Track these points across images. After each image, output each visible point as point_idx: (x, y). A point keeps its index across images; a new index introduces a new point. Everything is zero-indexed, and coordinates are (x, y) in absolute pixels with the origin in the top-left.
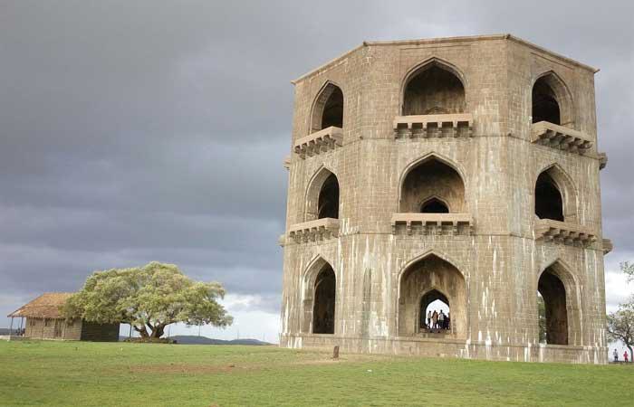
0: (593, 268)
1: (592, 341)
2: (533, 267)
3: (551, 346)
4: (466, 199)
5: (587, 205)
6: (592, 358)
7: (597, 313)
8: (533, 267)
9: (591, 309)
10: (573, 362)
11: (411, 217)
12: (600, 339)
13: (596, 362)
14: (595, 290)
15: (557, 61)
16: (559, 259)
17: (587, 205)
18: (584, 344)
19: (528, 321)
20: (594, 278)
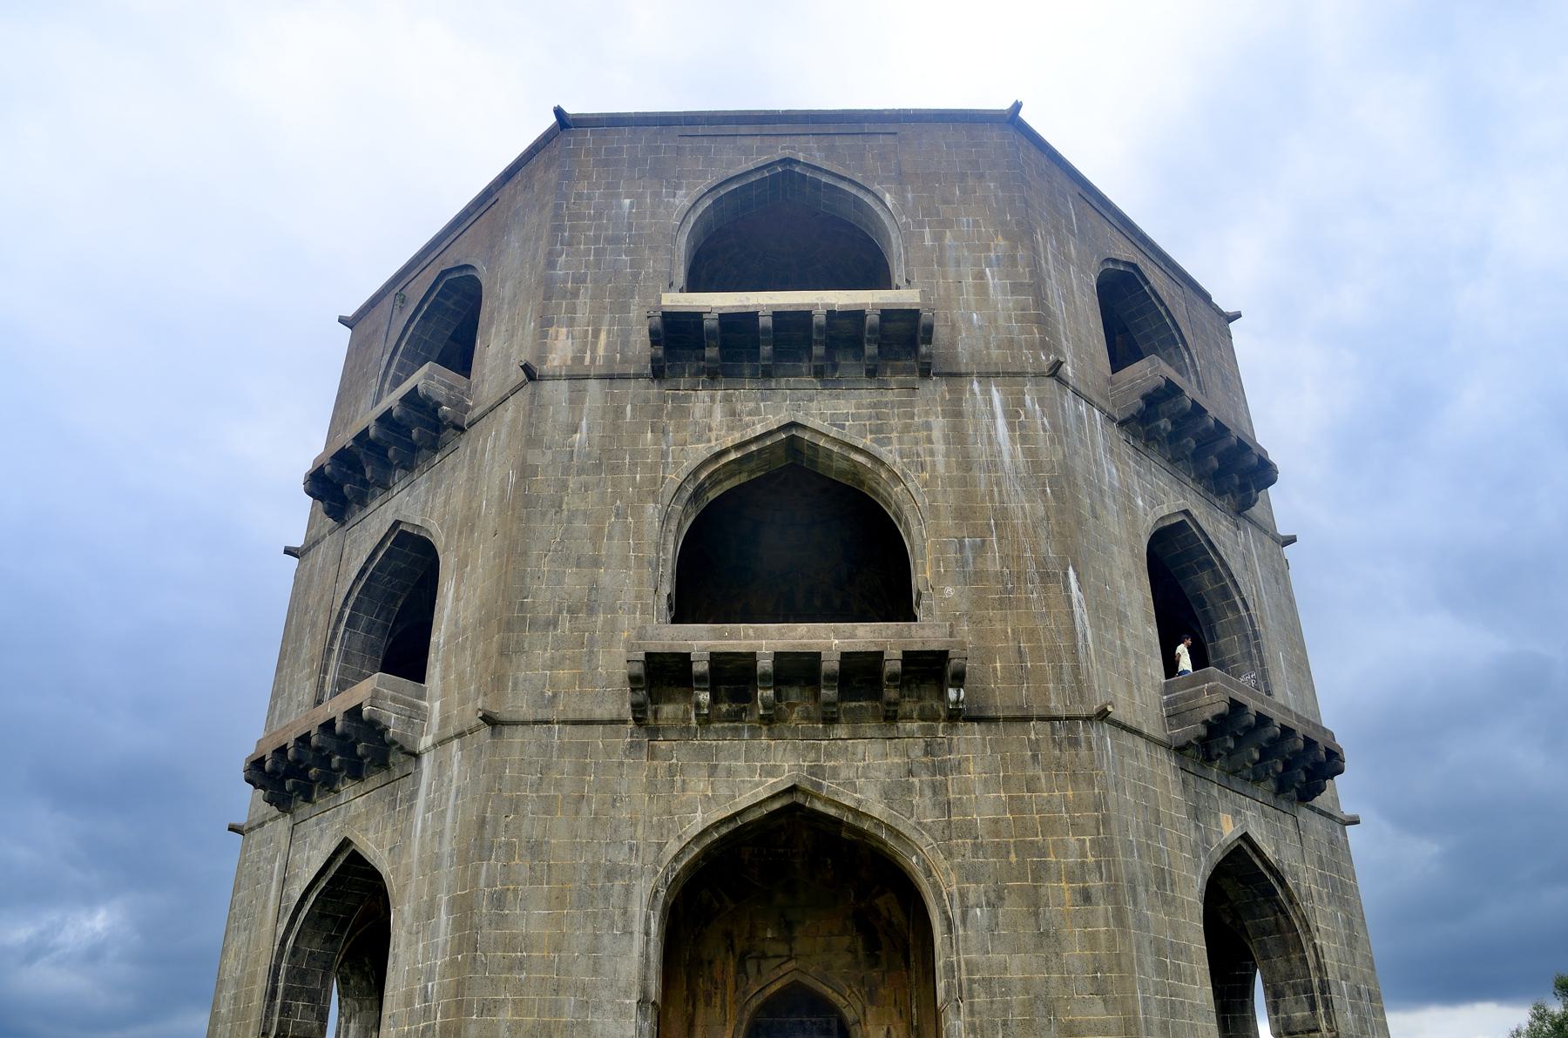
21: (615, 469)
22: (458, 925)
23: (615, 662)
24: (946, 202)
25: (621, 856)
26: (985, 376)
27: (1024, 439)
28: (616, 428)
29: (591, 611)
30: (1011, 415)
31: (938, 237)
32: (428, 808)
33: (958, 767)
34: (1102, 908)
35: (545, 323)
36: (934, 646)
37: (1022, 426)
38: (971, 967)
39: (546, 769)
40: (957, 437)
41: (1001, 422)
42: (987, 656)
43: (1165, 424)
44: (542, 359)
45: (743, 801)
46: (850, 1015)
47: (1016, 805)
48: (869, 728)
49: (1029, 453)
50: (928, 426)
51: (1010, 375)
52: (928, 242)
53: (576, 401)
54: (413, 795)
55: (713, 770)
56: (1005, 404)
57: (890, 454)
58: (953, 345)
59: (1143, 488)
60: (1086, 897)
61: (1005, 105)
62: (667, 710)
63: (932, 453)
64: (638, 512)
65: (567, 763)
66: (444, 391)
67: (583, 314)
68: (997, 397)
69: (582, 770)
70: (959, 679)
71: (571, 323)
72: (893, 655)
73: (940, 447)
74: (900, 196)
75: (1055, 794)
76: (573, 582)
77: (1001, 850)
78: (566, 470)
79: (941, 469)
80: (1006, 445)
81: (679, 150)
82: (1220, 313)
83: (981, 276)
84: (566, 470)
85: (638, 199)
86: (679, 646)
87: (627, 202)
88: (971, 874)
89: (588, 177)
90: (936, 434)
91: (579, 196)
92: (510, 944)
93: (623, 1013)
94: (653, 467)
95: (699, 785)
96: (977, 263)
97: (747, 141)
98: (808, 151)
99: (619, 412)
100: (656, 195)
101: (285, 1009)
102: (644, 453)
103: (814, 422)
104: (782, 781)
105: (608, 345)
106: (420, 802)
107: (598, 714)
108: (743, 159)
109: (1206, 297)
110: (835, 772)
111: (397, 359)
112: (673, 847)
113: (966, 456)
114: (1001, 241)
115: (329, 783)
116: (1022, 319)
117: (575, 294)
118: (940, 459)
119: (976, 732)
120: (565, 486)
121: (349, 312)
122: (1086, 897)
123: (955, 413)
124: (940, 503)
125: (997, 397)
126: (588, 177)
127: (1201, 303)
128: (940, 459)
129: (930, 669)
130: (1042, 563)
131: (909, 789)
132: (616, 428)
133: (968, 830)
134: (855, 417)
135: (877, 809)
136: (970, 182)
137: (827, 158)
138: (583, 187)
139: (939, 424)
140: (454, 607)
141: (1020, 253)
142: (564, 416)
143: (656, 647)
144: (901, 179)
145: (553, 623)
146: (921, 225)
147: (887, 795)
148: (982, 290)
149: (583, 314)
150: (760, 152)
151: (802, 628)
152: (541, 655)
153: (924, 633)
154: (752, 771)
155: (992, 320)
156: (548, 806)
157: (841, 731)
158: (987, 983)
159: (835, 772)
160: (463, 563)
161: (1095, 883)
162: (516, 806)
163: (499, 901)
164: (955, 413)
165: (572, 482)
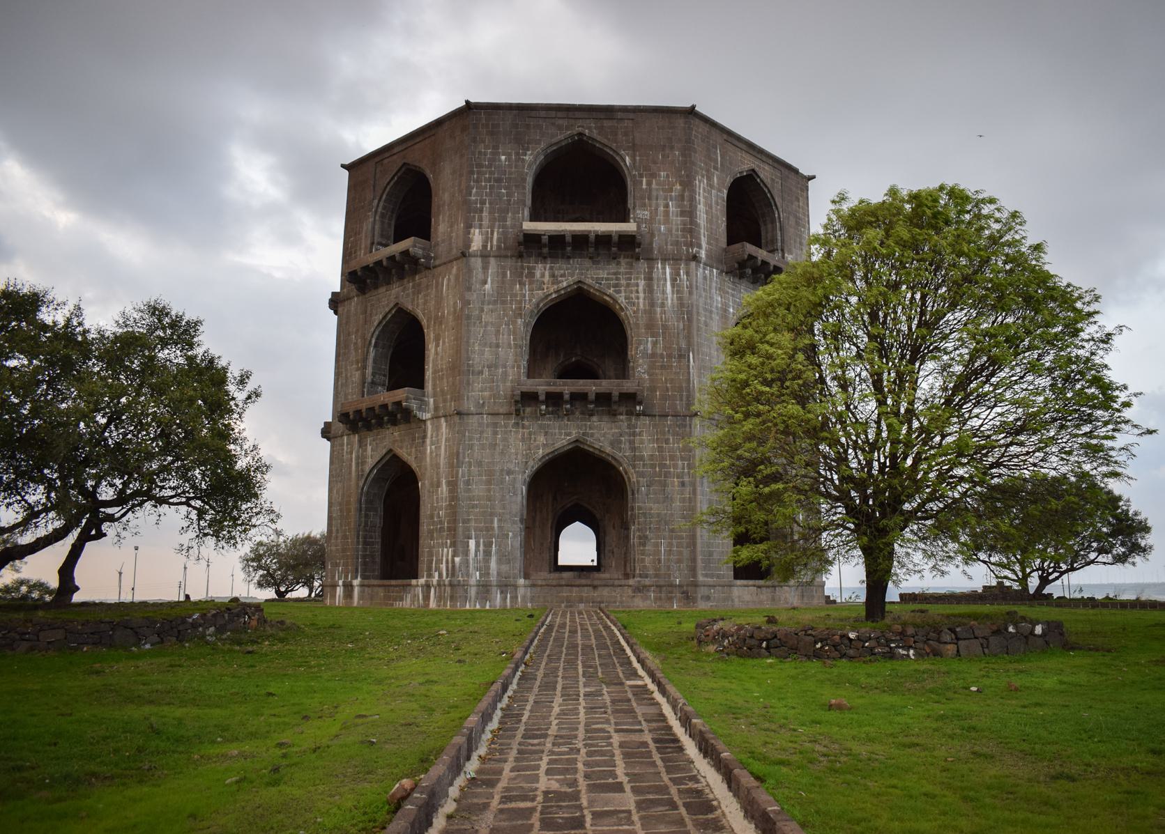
0: (438, 448)
1: (429, 569)
2: (354, 474)
3: (366, 582)
4: (760, 620)
5: (437, 345)
6: (426, 598)
7: (441, 522)
8: (354, 474)
9: (432, 517)
10: (398, 604)
11: (541, 386)
12: (444, 566)
13: (433, 604)
14: (439, 485)
15: (410, 144)
16: (735, 562)
17: (437, 345)
18: (533, 800)
19: (344, 550)
20: (438, 466)
21: (504, 302)
22: (451, 491)
23: (505, 388)
24: (655, 163)
25: (512, 467)
26: (664, 260)
27: (678, 292)
28: (503, 282)
29: (496, 367)
30: (673, 280)
31: (649, 184)
32: (432, 444)
33: (640, 434)
34: (688, 489)
35: (469, 226)
36: (631, 391)
37: (678, 286)
38: (640, 508)
39: (482, 432)
40: (649, 289)
41: (669, 283)
42: (653, 389)
43: (749, 271)
44: (469, 247)
45: (558, 445)
46: (598, 516)
47: (660, 449)
48: (605, 418)
49: (680, 299)
50: (637, 285)
51: (675, 259)
52: (644, 186)
53: (485, 268)
54: (424, 437)
55: (546, 434)
56: (671, 274)
57: (621, 299)
58: (651, 243)
59: (734, 302)
60: (683, 484)
61: (689, 105)
62: (528, 410)
63: (638, 298)
64: (514, 323)
65: (490, 430)
66: (420, 252)
67: (486, 222)
68: (668, 270)
69: (495, 433)
70: (640, 403)
71: (480, 227)
72: (615, 394)
73: (641, 295)
74: (633, 160)
75: (675, 445)
76: (488, 354)
77: (653, 466)
78: (483, 303)
79: (641, 306)
80: (670, 296)
81: (528, 126)
82: (803, 177)
83: (667, 206)
84: (483, 303)
85: (508, 155)
86: (533, 389)
87: (503, 158)
88: (641, 475)
89: (483, 142)
90: (641, 288)
91: (480, 153)
92: (471, 499)
93: (514, 523)
94: (520, 302)
95: (541, 439)
96: (666, 199)
97: (560, 122)
98: (590, 129)
99: (504, 275)
100: (517, 154)
101: (366, 516)
102: (516, 295)
103: (589, 281)
104: (573, 436)
105: (498, 239)
106: (428, 441)
107: (501, 411)
108: (560, 135)
109: (796, 171)
110: (592, 435)
111: (381, 204)
112: (531, 463)
113: (652, 299)
114: (678, 187)
115: (380, 425)
116: (683, 230)
117: (481, 211)
118: (641, 300)
119: (647, 420)
120: (482, 310)
121: (347, 163)
122: (683, 484)
123: (649, 279)
124: (640, 322)
125: (668, 270)
126: (483, 142)
127: (792, 175)
128: (641, 300)
129: (630, 399)
130: (680, 349)
131: (620, 442)
132: (503, 282)
133: (642, 458)
134: (607, 279)
135: (608, 449)
136: (667, 151)
137: (599, 134)
138: (481, 148)
139: (642, 283)
140: (436, 354)
141: (686, 194)
142: (480, 276)
143: (525, 389)
144: (633, 148)
145: (481, 372)
146: (641, 176)
147: (612, 444)
148: (667, 213)
149: (486, 222)
150: (567, 128)
151: (581, 381)
152: (478, 386)
153: (628, 386)
154: (560, 434)
155: (670, 231)
156: (483, 447)
157: (595, 418)
158: (644, 514)
159: (592, 435)
160: (437, 339)
161: (686, 479)
162: (471, 447)
163: (468, 483)
164: (649, 279)
165: (486, 308)
